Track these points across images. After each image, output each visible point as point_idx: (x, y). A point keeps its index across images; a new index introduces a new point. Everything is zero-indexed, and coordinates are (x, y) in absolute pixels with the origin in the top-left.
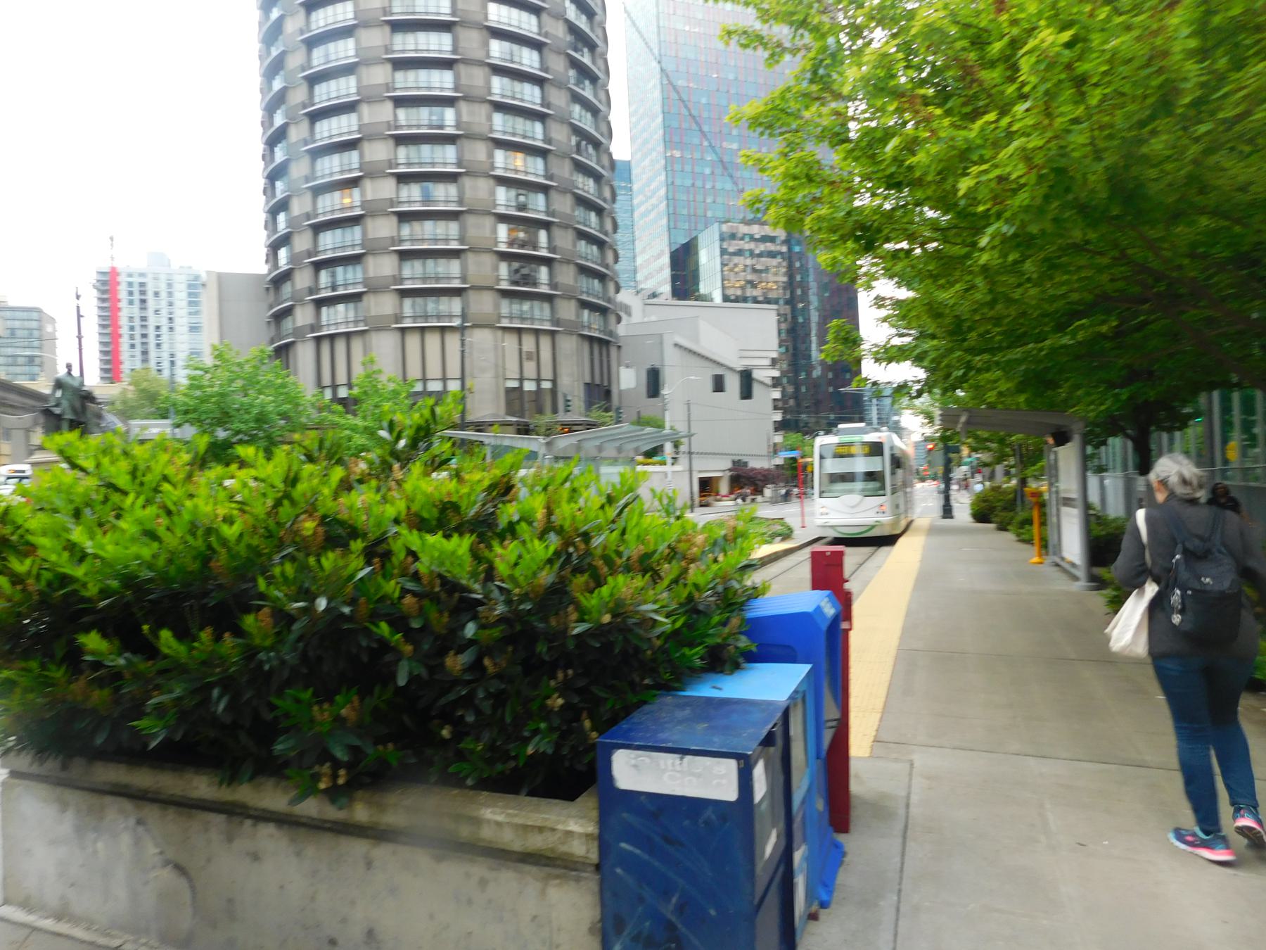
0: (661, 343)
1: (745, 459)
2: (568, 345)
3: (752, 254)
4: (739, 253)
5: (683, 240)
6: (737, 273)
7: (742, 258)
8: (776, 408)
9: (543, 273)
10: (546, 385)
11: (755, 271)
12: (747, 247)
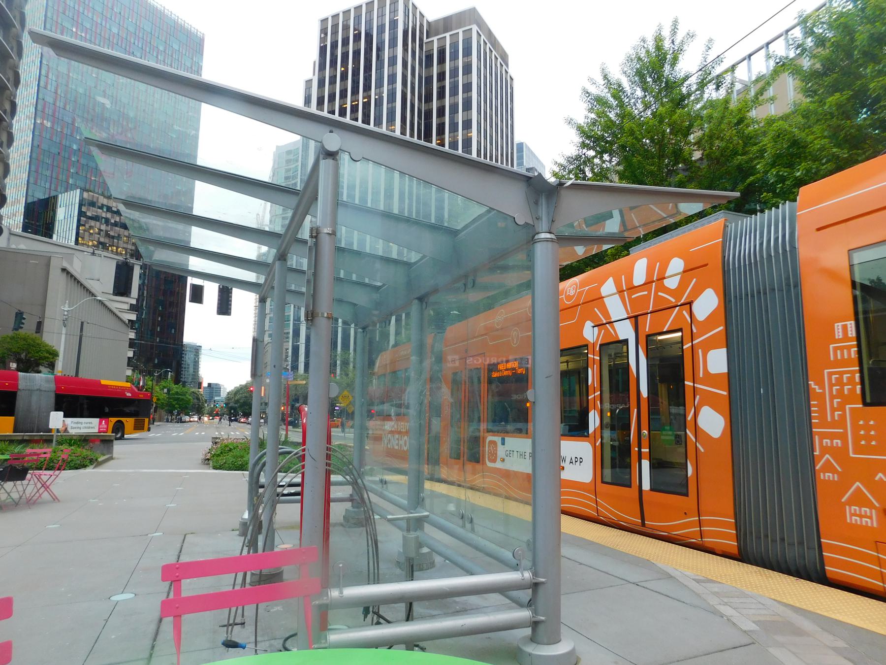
0: (48, 265)
3: (107, 221)
4: (96, 218)
5: (40, 195)
6: (91, 234)
7: (98, 223)
11: (107, 235)
12: (104, 215)
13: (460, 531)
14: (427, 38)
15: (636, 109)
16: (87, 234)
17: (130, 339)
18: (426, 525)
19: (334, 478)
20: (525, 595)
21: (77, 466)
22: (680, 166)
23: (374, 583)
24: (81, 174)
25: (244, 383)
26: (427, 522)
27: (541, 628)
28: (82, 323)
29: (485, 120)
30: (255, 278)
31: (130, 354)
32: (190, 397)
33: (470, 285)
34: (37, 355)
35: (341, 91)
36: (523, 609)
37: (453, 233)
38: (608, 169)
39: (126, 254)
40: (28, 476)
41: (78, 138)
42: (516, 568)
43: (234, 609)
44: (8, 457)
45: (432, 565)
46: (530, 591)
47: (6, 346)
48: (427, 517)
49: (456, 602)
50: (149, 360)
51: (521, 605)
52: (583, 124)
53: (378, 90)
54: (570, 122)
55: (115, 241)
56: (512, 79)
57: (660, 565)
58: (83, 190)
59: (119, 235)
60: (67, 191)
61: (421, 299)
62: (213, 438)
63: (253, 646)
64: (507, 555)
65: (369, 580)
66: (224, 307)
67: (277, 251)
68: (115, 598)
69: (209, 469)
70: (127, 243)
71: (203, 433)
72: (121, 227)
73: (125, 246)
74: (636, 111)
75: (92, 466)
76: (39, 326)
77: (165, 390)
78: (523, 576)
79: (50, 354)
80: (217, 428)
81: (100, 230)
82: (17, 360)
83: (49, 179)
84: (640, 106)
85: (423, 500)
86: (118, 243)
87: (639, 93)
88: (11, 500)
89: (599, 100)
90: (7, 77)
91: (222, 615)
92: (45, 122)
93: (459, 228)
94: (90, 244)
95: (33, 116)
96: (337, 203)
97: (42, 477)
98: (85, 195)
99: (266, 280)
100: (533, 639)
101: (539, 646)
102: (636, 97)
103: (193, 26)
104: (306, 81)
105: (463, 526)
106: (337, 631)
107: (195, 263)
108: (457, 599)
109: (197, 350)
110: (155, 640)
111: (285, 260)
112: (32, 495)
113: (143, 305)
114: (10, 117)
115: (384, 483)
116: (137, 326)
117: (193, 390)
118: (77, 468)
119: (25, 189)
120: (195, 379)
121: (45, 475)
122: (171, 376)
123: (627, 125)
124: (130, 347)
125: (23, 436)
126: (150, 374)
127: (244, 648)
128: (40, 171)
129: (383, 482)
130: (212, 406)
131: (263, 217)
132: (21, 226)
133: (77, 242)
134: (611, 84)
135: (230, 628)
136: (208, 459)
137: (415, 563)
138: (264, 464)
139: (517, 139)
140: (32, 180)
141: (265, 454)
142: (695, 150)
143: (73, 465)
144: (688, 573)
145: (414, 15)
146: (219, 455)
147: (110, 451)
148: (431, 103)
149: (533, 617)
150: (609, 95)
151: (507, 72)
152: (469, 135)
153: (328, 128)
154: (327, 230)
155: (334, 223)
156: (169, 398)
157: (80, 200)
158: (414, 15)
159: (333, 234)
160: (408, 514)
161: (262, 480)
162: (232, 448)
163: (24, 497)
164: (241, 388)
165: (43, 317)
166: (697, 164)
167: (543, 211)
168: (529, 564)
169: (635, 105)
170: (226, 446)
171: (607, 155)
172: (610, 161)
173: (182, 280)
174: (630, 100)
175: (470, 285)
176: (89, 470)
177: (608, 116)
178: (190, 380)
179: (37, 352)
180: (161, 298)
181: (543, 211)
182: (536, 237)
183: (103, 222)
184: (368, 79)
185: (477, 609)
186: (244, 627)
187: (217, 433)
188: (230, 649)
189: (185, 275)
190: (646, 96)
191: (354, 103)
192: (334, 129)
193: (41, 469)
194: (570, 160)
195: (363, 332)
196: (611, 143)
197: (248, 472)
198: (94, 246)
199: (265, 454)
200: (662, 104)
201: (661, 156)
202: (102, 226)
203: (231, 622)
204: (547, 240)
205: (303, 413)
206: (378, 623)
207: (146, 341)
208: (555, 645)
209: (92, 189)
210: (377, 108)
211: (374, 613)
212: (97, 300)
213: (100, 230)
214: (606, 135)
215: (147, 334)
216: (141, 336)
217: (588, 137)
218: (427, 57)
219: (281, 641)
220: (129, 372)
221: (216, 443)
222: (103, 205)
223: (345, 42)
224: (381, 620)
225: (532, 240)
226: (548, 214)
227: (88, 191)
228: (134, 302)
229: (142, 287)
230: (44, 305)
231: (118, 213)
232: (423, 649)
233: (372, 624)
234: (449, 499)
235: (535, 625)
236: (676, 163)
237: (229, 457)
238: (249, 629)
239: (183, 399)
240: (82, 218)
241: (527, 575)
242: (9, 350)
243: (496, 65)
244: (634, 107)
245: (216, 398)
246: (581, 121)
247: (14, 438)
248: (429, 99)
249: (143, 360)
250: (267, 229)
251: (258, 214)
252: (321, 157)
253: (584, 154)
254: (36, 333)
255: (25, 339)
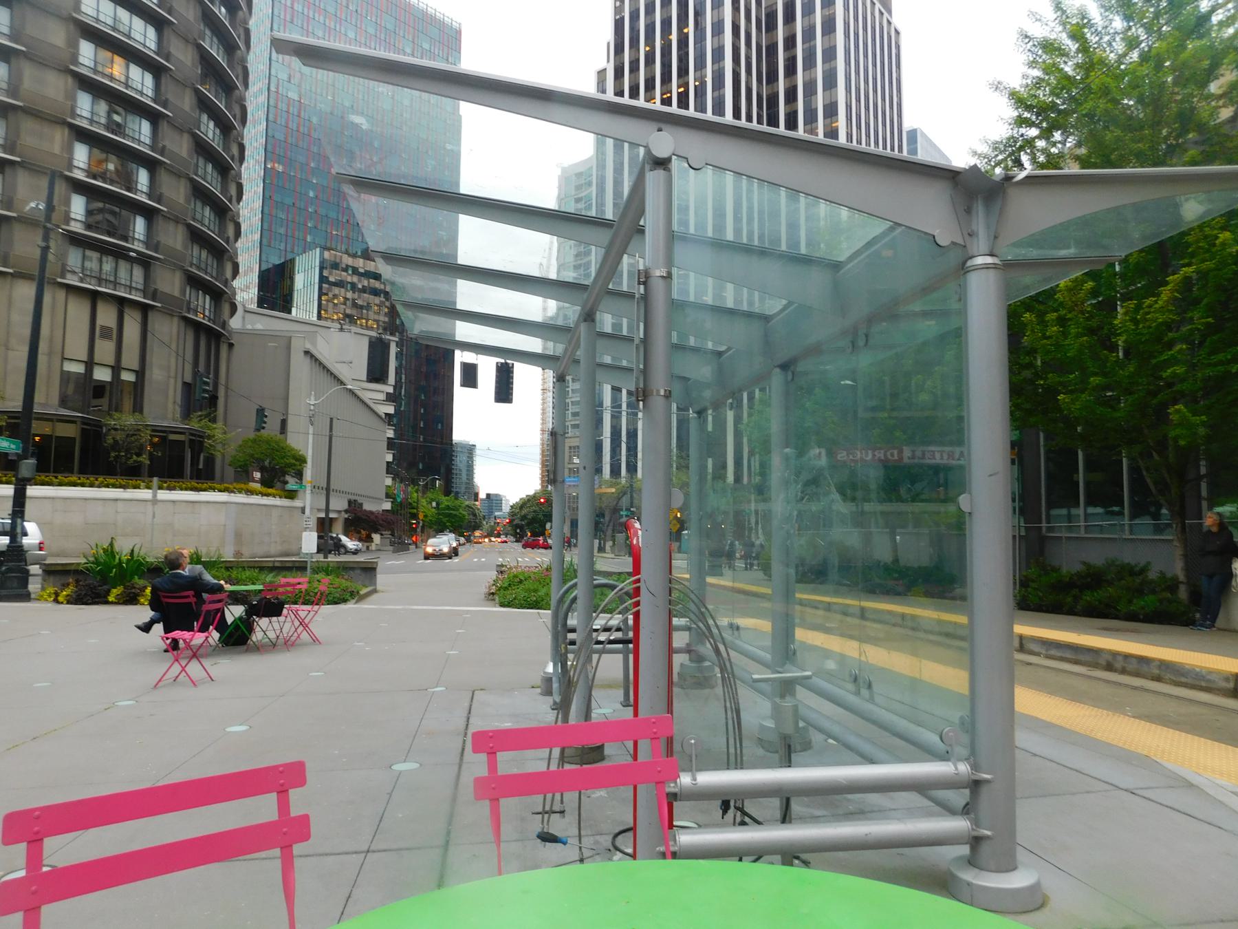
0: (289, 348)
1: (360, 500)
2: (165, 329)
3: (354, 287)
4: (340, 284)
6: (335, 305)
7: (343, 290)
8: (388, 496)
9: (140, 225)
10: (127, 377)
11: (355, 305)
12: (349, 279)
13: (852, 699)
15: (1112, 52)
16: (330, 305)
17: (388, 438)
18: (798, 688)
19: (675, 621)
20: (959, 798)
21: (336, 600)
22: (1191, 136)
23: (736, 768)
24: (319, 227)
25: (531, 493)
26: (799, 684)
27: (985, 848)
28: (331, 420)
29: (858, 100)
30: (541, 347)
31: (389, 458)
32: (464, 513)
33: (861, 343)
34: (282, 461)
35: (646, 81)
36: (956, 817)
37: (836, 266)
38: (1061, 155)
39: (378, 328)
40: (285, 611)
41: (314, 181)
42: (944, 757)
43: (549, 796)
44: (261, 587)
45: (807, 746)
46: (967, 792)
47: (250, 451)
48: (808, 678)
49: (849, 800)
50: (412, 465)
51: (951, 811)
52: (1018, 88)
53: (698, 73)
54: (997, 86)
55: (365, 311)
56: (897, 32)
57: (1169, 766)
58: (325, 248)
59: (368, 303)
60: (305, 252)
61: (785, 367)
62: (498, 566)
63: (576, 841)
64: (932, 738)
65: (728, 764)
66: (504, 392)
67: (582, 309)
68: (398, 767)
69: (495, 607)
70: (378, 313)
71: (483, 560)
72: (370, 293)
73: (376, 317)
74: (1112, 55)
75: (354, 601)
76: (284, 423)
77: (434, 504)
78: (956, 769)
79: (297, 460)
80: (500, 552)
81: (346, 299)
82: (260, 469)
84: (1119, 46)
85: (794, 653)
86: (368, 314)
87: (1118, 23)
88: (267, 640)
89: (1049, 46)
90: (233, 113)
91: (536, 801)
92: (276, 165)
93: (842, 259)
94: (335, 317)
95: (263, 159)
96: (671, 237)
97: (299, 612)
98: (327, 254)
99: (566, 350)
100: (972, 862)
101: (983, 872)
102: (1112, 31)
103: (446, 15)
104: (598, 72)
105: (858, 693)
106: (688, 831)
107: (465, 331)
108: (850, 796)
109: (470, 450)
110: (450, 823)
111: (593, 320)
112: (290, 635)
113: (400, 393)
114: (238, 164)
115: (735, 629)
116: (395, 420)
117: (467, 503)
118: (336, 603)
119: (258, 253)
120: (469, 488)
121: (303, 610)
122: (440, 484)
123: (1096, 80)
124: (388, 449)
125: (274, 562)
126: (414, 482)
127: (565, 843)
129: (735, 628)
130: (492, 524)
131: (548, 268)
132: (256, 301)
133: (319, 317)
134: (1068, 17)
135: (546, 816)
136: (493, 594)
137: (675, 738)
138: (575, 599)
139: (907, 125)
141: (575, 585)
142: (1220, 107)
143: (331, 599)
144: (1223, 782)
146: (506, 589)
147: (373, 580)
148: (776, 84)
149: (973, 829)
150: (1064, 36)
151: (889, 23)
152: (834, 125)
153: (655, 126)
154: (659, 272)
155: (669, 262)
156: (439, 514)
157: (320, 262)
159: (669, 276)
160: (773, 673)
161: (572, 622)
162: (523, 579)
163: (281, 637)
164: (529, 500)
165: (286, 414)
166: (1223, 130)
167: (980, 223)
168: (964, 752)
169: (1110, 44)
170: (515, 576)
171: (1059, 132)
172: (1064, 143)
173: (448, 357)
174: (1101, 38)
175: (861, 343)
176: (350, 606)
177: (1062, 69)
178: (463, 490)
179: (282, 458)
180: (423, 383)
181: (980, 223)
182: (969, 263)
184: (683, 59)
185: (880, 811)
186: (564, 817)
187: (501, 560)
188: (547, 843)
189: (452, 348)
190: (1130, 28)
191: (665, 96)
192: (663, 126)
193: (296, 603)
194: (995, 146)
195: (700, 418)
196: (1066, 113)
197: (549, 612)
198: (338, 319)
199: (575, 585)
200: (1161, 37)
201: (1156, 124)
202: (348, 293)
203: (547, 808)
204: (986, 267)
205: (632, 531)
206: (743, 823)
207: (408, 440)
208: (1012, 873)
209: (334, 246)
211: (737, 808)
212: (347, 389)
213: (346, 299)
214: (1058, 102)
215: (408, 431)
216: (401, 434)
217: (1029, 108)
218: (767, 15)
219: (610, 838)
220: (389, 481)
221: (502, 572)
222: (347, 266)
224: (747, 819)
225: (963, 269)
226: (988, 227)
227: (329, 249)
228: (391, 390)
229: (399, 371)
230: (286, 399)
231: (377, 277)
232: (806, 864)
233: (734, 824)
234: (827, 654)
235: (976, 841)
236: (1184, 131)
237: (520, 592)
238: (571, 818)
239: (455, 515)
240: (324, 285)
241: (963, 768)
242: (252, 456)
243: (873, 14)
244: (1108, 49)
245: (497, 514)
246: (1016, 83)
247: (264, 565)
248: (772, 77)
249: (405, 465)
250: (553, 275)
251: (541, 264)
252: (647, 167)
253: (1022, 135)
254: (281, 433)
255: (268, 442)
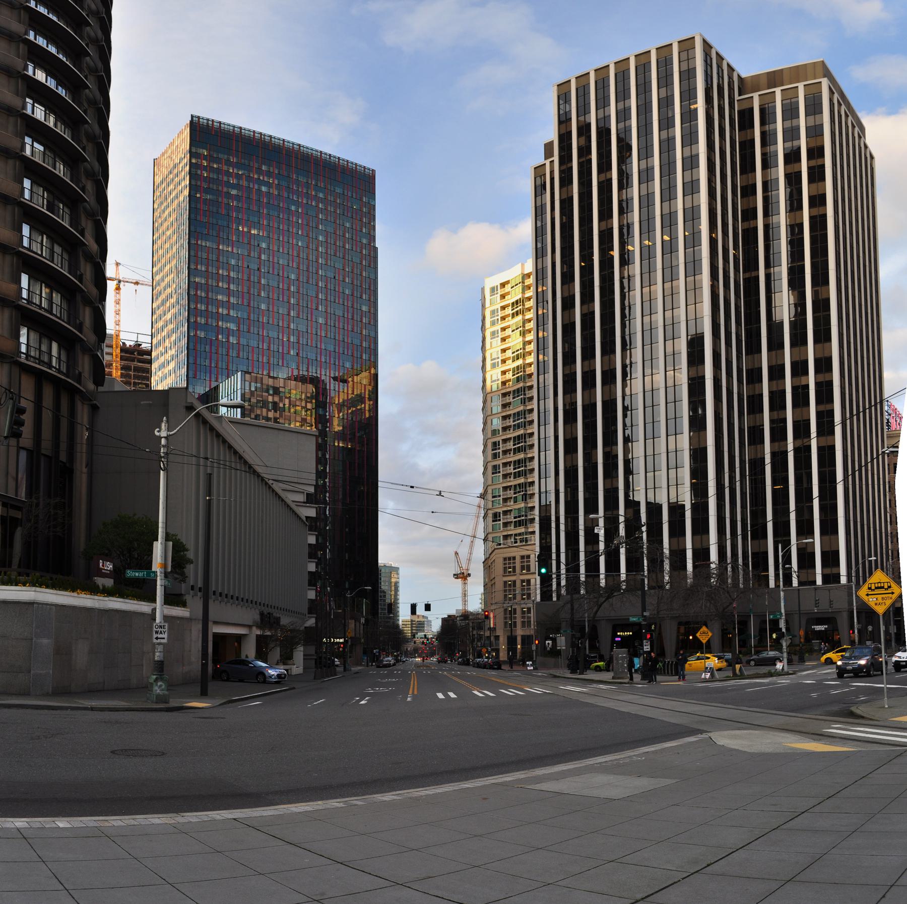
7: (264, 410)
8: (310, 611)
14: (740, 95)
83: (208, 368)
128: (198, 362)
140: (191, 375)
145: (719, 67)
158: (719, 67)
183: (270, 408)
197: (239, 416)
210: (667, 256)
223: (670, 248)
243: (854, 138)
